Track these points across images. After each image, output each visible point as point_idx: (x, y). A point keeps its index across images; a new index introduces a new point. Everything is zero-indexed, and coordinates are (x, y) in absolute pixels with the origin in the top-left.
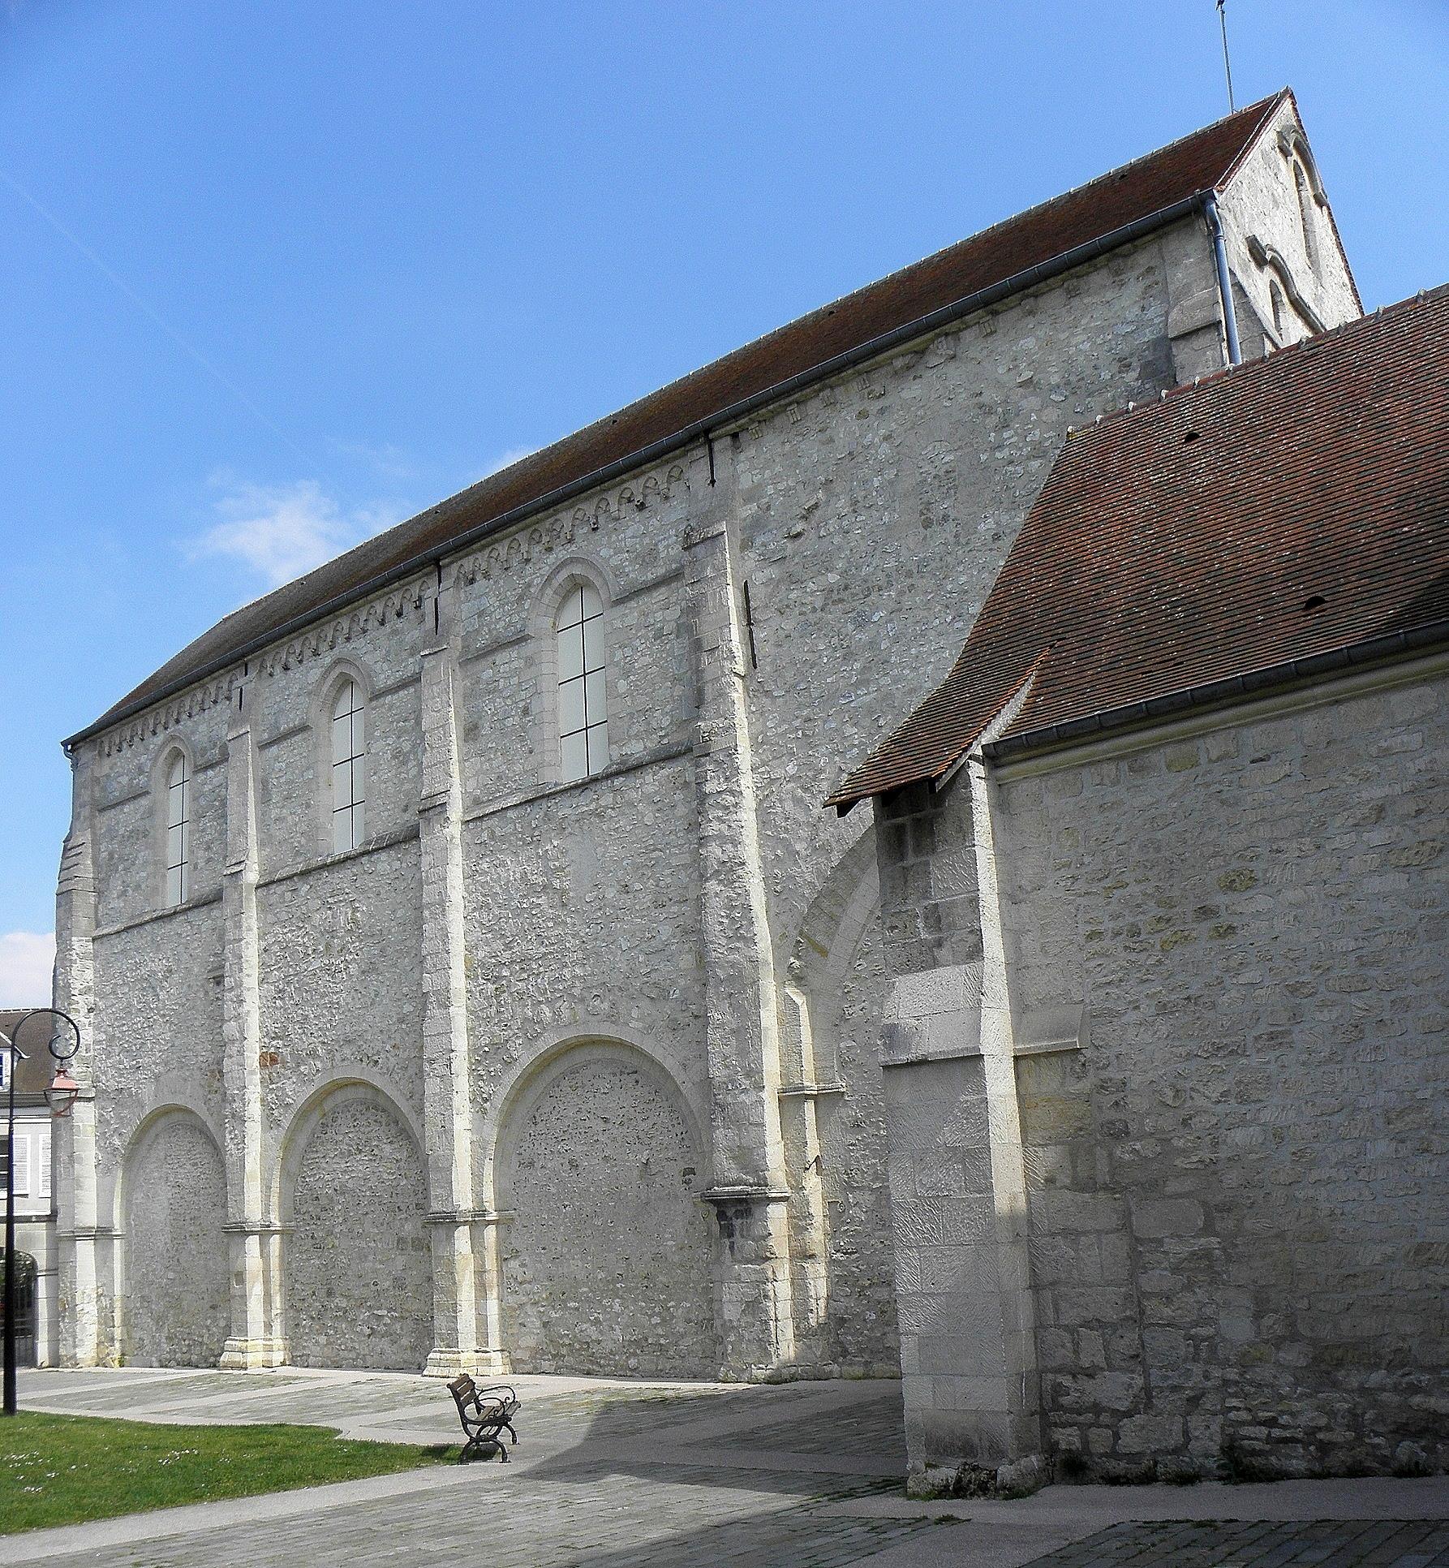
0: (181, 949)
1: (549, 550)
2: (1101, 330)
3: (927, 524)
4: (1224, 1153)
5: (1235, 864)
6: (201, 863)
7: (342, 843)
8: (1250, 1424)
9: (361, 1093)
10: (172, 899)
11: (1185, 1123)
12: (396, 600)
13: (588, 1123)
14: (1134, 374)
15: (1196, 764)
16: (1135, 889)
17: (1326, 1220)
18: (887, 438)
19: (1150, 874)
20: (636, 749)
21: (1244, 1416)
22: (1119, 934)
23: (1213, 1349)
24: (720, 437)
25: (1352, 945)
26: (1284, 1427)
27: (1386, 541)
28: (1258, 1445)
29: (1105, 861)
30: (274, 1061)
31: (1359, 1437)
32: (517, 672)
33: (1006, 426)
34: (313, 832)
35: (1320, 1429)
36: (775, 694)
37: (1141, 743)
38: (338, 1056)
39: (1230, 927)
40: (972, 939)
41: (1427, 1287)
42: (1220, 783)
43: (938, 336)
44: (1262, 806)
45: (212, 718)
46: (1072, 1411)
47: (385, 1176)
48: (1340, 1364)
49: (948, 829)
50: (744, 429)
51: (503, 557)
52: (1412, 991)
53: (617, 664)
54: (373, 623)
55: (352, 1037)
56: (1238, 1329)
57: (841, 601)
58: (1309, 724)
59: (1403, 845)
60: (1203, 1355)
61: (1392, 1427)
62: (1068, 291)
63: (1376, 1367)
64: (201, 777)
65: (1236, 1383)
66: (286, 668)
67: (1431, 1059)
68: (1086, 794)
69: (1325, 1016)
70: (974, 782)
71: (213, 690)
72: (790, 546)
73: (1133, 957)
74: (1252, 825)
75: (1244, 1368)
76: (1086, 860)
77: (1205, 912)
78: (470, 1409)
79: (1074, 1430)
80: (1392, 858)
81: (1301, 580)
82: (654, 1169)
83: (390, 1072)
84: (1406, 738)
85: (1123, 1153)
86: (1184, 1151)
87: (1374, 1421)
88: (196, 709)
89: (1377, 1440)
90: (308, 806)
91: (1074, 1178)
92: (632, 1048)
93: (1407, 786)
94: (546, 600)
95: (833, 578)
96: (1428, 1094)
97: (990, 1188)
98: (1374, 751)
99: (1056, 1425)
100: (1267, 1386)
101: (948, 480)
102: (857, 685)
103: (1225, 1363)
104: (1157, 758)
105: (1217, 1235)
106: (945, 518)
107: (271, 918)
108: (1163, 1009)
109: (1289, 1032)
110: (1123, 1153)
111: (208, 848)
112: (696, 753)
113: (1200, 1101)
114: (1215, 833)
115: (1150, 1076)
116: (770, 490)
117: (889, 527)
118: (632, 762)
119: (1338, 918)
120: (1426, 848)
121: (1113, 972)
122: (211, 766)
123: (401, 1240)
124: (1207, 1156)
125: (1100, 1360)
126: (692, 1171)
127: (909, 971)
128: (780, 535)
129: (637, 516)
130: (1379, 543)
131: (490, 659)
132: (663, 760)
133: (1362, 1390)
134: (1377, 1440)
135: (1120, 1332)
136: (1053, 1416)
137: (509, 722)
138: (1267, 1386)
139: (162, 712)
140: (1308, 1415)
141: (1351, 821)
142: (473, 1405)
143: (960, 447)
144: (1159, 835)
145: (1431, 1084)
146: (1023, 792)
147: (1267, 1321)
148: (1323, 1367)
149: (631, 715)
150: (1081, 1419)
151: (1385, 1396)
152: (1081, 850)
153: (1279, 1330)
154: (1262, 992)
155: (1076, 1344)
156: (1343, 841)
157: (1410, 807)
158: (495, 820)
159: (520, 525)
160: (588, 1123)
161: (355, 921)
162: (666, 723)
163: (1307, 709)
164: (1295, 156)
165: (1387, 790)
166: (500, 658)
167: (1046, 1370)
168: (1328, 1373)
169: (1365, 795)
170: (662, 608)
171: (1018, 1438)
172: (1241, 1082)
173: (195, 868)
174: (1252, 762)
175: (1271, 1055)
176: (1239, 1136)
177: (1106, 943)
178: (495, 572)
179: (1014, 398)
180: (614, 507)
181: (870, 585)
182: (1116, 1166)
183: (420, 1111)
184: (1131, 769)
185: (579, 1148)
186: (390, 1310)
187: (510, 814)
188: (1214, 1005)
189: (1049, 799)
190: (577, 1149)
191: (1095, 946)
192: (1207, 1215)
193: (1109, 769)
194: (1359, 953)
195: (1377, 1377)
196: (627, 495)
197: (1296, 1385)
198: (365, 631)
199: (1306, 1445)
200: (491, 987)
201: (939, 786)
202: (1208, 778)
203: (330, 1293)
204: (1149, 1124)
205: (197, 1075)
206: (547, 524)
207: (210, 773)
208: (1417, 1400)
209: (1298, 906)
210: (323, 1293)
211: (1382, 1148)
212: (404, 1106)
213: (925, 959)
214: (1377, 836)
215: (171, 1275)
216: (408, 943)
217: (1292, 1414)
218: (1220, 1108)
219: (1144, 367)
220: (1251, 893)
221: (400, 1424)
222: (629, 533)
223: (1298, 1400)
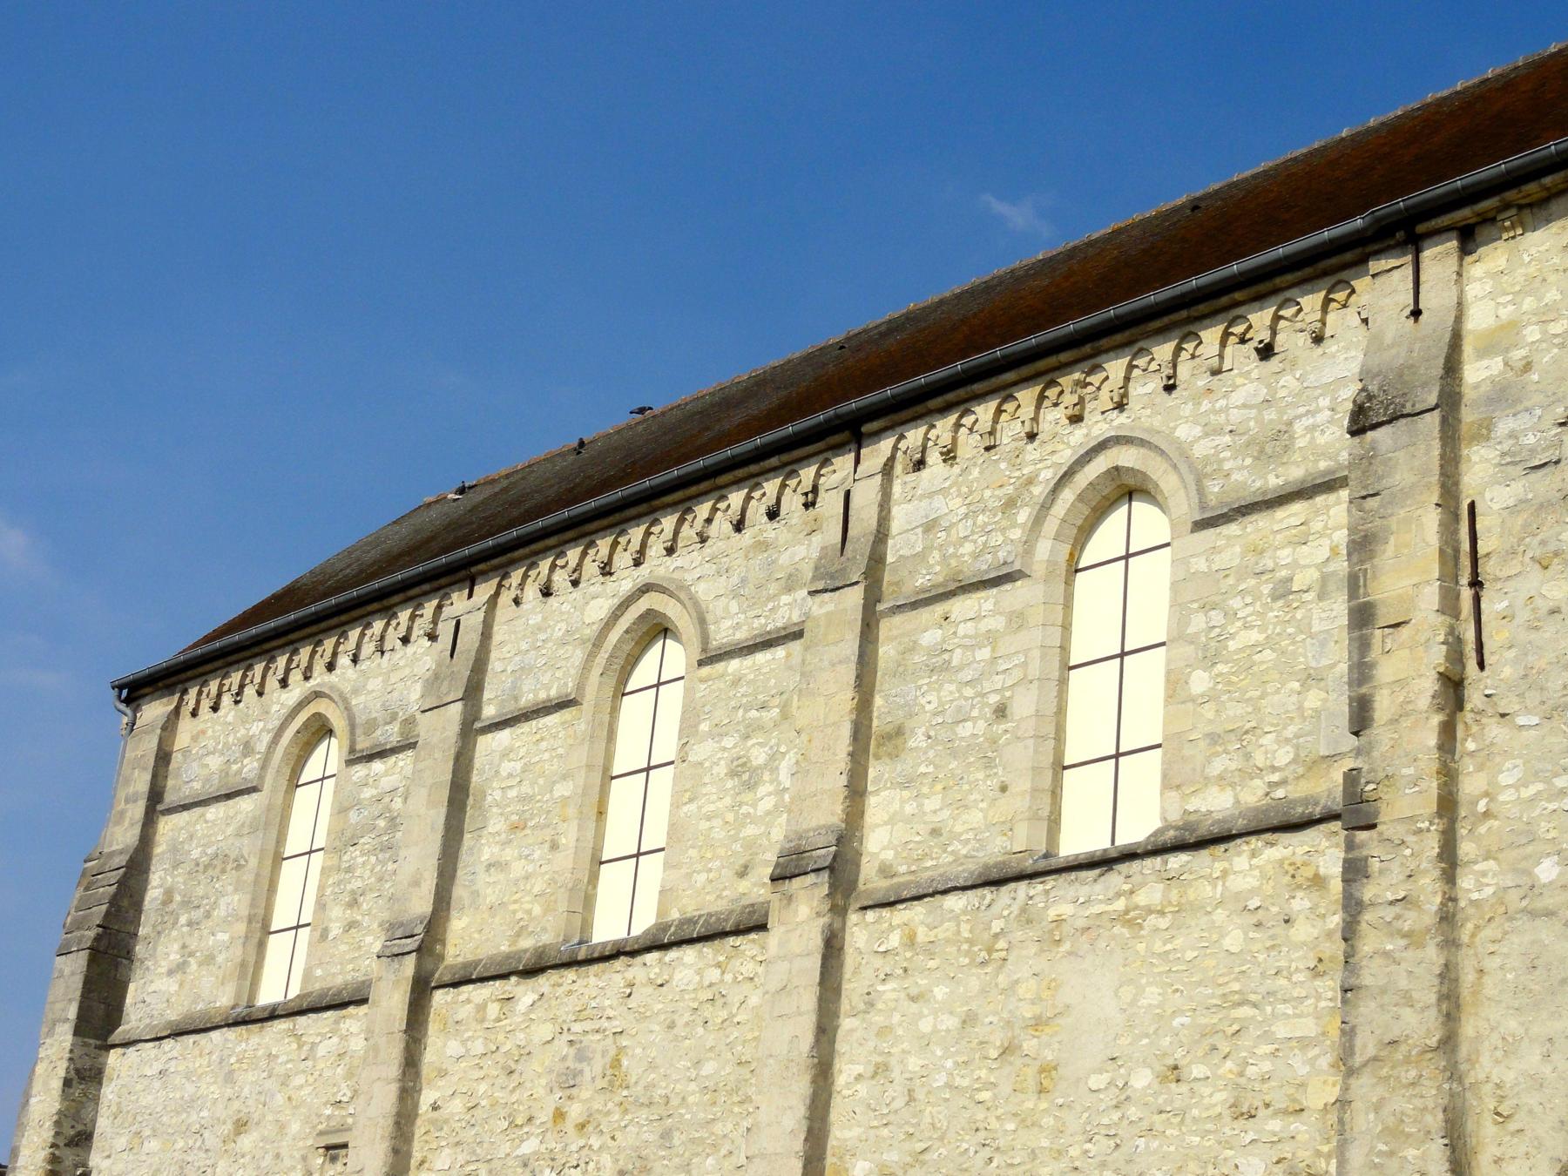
1: (1076, 419)
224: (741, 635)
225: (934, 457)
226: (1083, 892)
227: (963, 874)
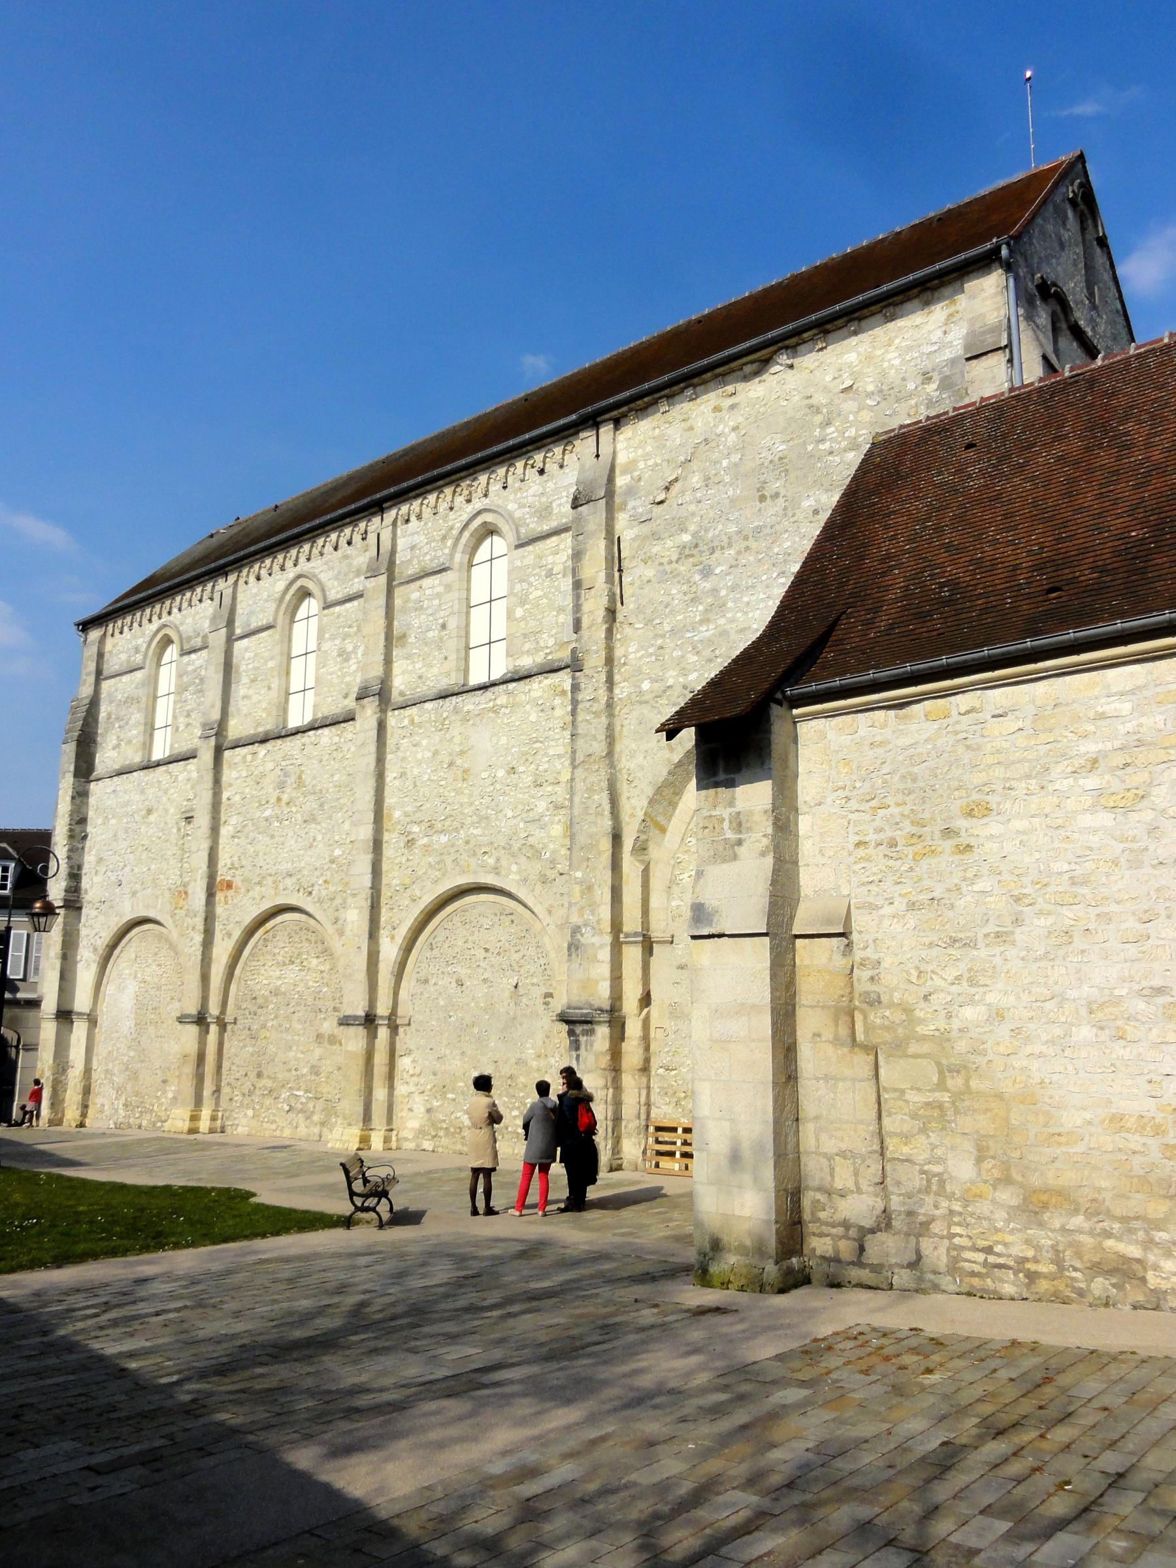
2: (910, 349)
3: (762, 498)
4: (956, 1024)
5: (975, 796)
11: (926, 998)
13: (472, 952)
14: (934, 386)
16: (894, 810)
18: (735, 429)
19: (907, 799)
20: (526, 662)
21: (964, 1242)
23: (942, 1183)
24: (605, 421)
25: (1066, 867)
26: (998, 1255)
27: (1116, 543)
28: (977, 1268)
29: (873, 786)
32: (439, 595)
33: (828, 424)
35: (1027, 1260)
36: (637, 626)
38: (281, 887)
39: (968, 846)
41: (1120, 1150)
42: (966, 731)
43: (781, 348)
44: (998, 752)
45: (198, 613)
46: (827, 1224)
47: (311, 983)
50: (625, 416)
53: (515, 595)
57: (692, 556)
59: (1112, 790)
60: (934, 1188)
61: (1088, 1265)
62: (885, 315)
64: (186, 659)
65: (960, 1214)
66: (258, 579)
67: (1127, 965)
69: (1042, 922)
73: (891, 863)
74: (990, 766)
75: (966, 1203)
76: (858, 785)
77: (948, 832)
78: (358, 1186)
79: (828, 1240)
80: (1103, 801)
81: (1044, 571)
82: (521, 990)
83: (320, 901)
84: (1118, 705)
89: (1074, 1274)
95: (686, 538)
98: (1091, 715)
99: (814, 1234)
100: (985, 1219)
101: (781, 465)
102: (702, 622)
103: (951, 1197)
105: (948, 1091)
106: (777, 495)
108: (912, 906)
111: (188, 715)
113: (938, 982)
114: (960, 771)
116: (641, 465)
117: (732, 501)
118: (523, 673)
120: (1130, 795)
121: (874, 874)
122: (195, 651)
123: (319, 1037)
124: (942, 1025)
125: (850, 1184)
126: (550, 995)
128: (647, 503)
130: (1110, 544)
131: (418, 583)
133: (1063, 1230)
134: (1074, 1274)
135: (867, 1163)
137: (430, 634)
138: (985, 1219)
141: (1070, 769)
142: (361, 1181)
143: (792, 439)
144: (916, 770)
145: (1126, 985)
147: (987, 1164)
149: (525, 636)
150: (834, 1231)
151: (1083, 1238)
152: (854, 778)
153: (996, 1173)
154: (991, 899)
155: (832, 1169)
156: (1064, 784)
157: (1119, 760)
159: (447, 480)
160: (472, 952)
162: (551, 642)
164: (1082, 207)
165: (1100, 746)
166: (427, 582)
168: (1036, 1213)
169: (1083, 749)
173: (177, 729)
174: (993, 717)
175: (997, 950)
177: (870, 850)
179: (836, 401)
181: (715, 544)
186: (306, 1091)
188: (952, 906)
190: (463, 971)
191: (861, 852)
195: (1078, 1221)
202: (958, 727)
203: (259, 1075)
204: (897, 997)
205: (167, 894)
207: (193, 656)
208: (1110, 1243)
209: (1024, 833)
210: (252, 1075)
211: (1085, 1032)
214: (1091, 782)
215: (132, 1054)
216: (342, 801)
217: (1005, 1245)
218: (954, 989)
219: (942, 381)
220: (985, 820)
221: (303, 1190)
222: (531, 492)
223: (1012, 1232)
225: (413, 518)
226: (477, 700)
227: (432, 693)
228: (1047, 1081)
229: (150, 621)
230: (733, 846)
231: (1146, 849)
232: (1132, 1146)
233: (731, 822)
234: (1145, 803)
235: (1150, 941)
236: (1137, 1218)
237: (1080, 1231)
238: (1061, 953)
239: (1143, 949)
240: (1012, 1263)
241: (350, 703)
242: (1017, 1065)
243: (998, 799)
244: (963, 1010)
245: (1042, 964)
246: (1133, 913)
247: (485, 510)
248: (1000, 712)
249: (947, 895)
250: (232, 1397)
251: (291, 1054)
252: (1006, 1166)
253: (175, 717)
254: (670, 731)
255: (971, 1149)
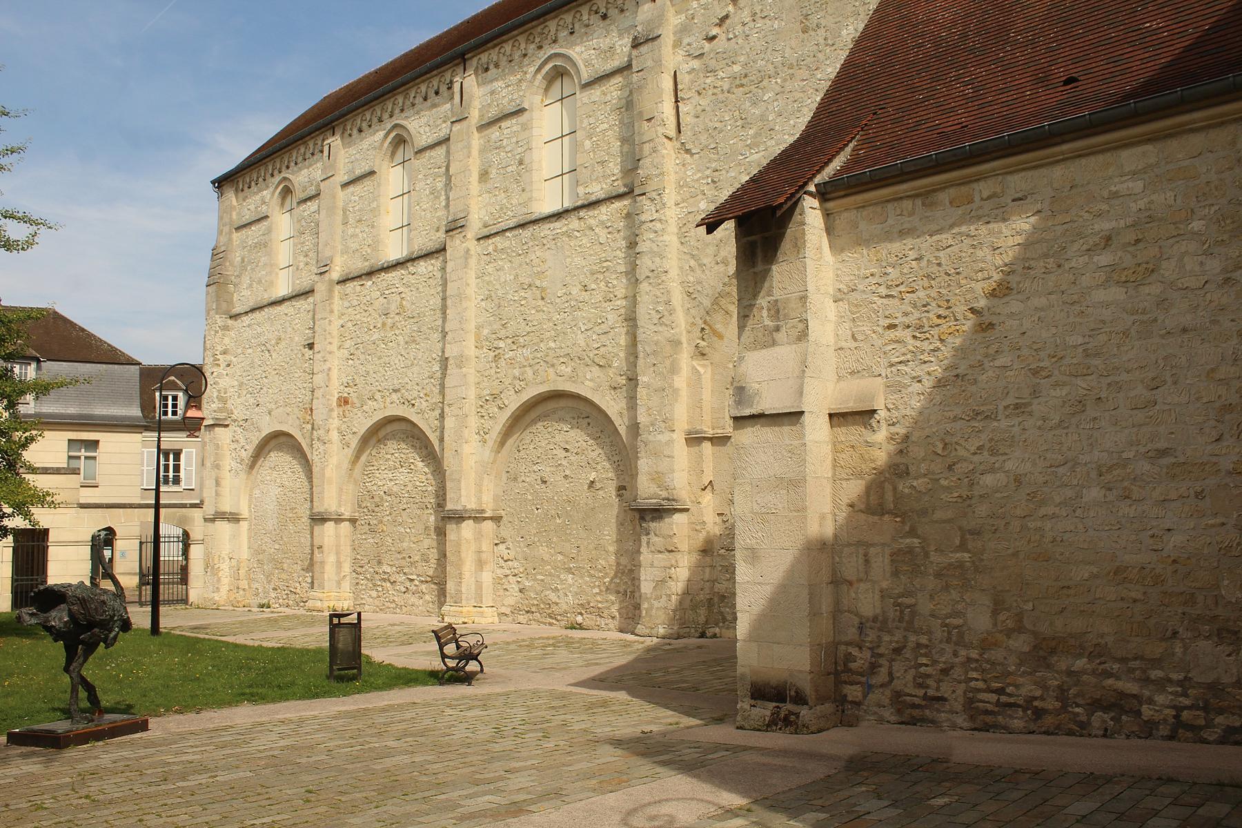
0: (287, 324)
1: (540, 47)
4: (977, 491)
6: (302, 265)
7: (394, 251)
8: (984, 691)
9: (403, 426)
10: (282, 290)
11: (950, 468)
12: (435, 82)
15: (971, 201)
17: (1050, 545)
20: (597, 190)
21: (981, 685)
22: (908, 327)
25: (1080, 340)
26: (1010, 695)
30: (346, 402)
31: (1064, 707)
34: (375, 245)
35: (1036, 698)
37: (926, 186)
38: (388, 400)
40: (801, 326)
41: (1122, 599)
48: (1053, 651)
49: (786, 245)
51: (508, 53)
52: (1124, 376)
53: (585, 129)
54: (419, 100)
55: (397, 387)
56: (980, 620)
57: (742, 85)
58: (1057, 172)
59: (1124, 265)
60: (954, 639)
63: (1080, 656)
65: (977, 661)
66: (360, 131)
67: (1135, 429)
68: (890, 222)
69: (1058, 393)
70: (808, 211)
71: (311, 145)
72: (707, 45)
73: (918, 344)
82: (598, 485)
84: (1131, 184)
85: (903, 487)
86: (948, 488)
87: (1076, 696)
88: (300, 159)
89: (1077, 710)
90: (373, 227)
91: (868, 504)
92: (586, 400)
93: (1129, 221)
94: (537, 83)
96: (1131, 455)
97: (804, 509)
99: (845, 683)
103: (967, 646)
104: (944, 197)
105: (969, 552)
107: (346, 304)
109: (1030, 404)
110: (903, 487)
112: (637, 192)
113: (961, 452)
115: (927, 432)
118: (593, 198)
119: (1071, 319)
122: (310, 199)
126: (624, 488)
127: (755, 349)
129: (602, 24)
132: (614, 197)
133: (1070, 673)
134: (1077, 710)
136: (844, 677)
139: (278, 161)
140: (1027, 688)
145: (1134, 448)
146: (842, 220)
147: (1001, 617)
148: (1041, 653)
153: (1010, 624)
154: (1012, 373)
157: (1131, 236)
158: (498, 238)
159: (520, 30)
161: (402, 306)
163: (1058, 162)
165: (1114, 224)
166: (504, 124)
167: (840, 643)
168: (1045, 658)
170: (613, 90)
171: (816, 691)
172: (992, 439)
175: (1016, 421)
176: (988, 479)
177: (898, 333)
178: (503, 62)
180: (585, 17)
182: (898, 498)
183: (442, 440)
184: (923, 204)
185: (548, 469)
187: (508, 234)
189: (863, 225)
190: (546, 470)
191: (892, 334)
192: (962, 537)
193: (907, 204)
194: (1085, 347)
195: (1081, 663)
196: (594, 8)
197: (1020, 665)
198: (413, 105)
199: (1025, 710)
200: (492, 354)
201: (779, 213)
202: (980, 212)
206: (539, 29)
208: (1110, 681)
209: (1042, 309)
211: (1095, 493)
212: (433, 438)
213: (769, 340)
214: (1104, 259)
215: (277, 547)
217: (1017, 686)
218: (976, 459)
223: (1021, 676)
224: (430, 141)
225: (491, 66)
226: (552, 226)
227: (511, 223)
228: (1059, 539)
229: (272, 175)
230: (771, 333)
231: (1155, 320)
232: (1133, 595)
233: (769, 310)
234: (1155, 276)
235: (1157, 407)
236: (1135, 659)
237: (1084, 672)
238: (1074, 421)
239: (1151, 413)
240: (1021, 702)
241: (441, 234)
242: (1031, 525)
243: (1018, 279)
244: (983, 478)
245: (1057, 432)
246: (1142, 381)
247: (556, 55)
248: (1019, 195)
249: (970, 372)
250: (778, 761)
251: (405, 545)
252: (1019, 617)
253: (295, 258)
254: (711, 225)
255: (987, 603)
